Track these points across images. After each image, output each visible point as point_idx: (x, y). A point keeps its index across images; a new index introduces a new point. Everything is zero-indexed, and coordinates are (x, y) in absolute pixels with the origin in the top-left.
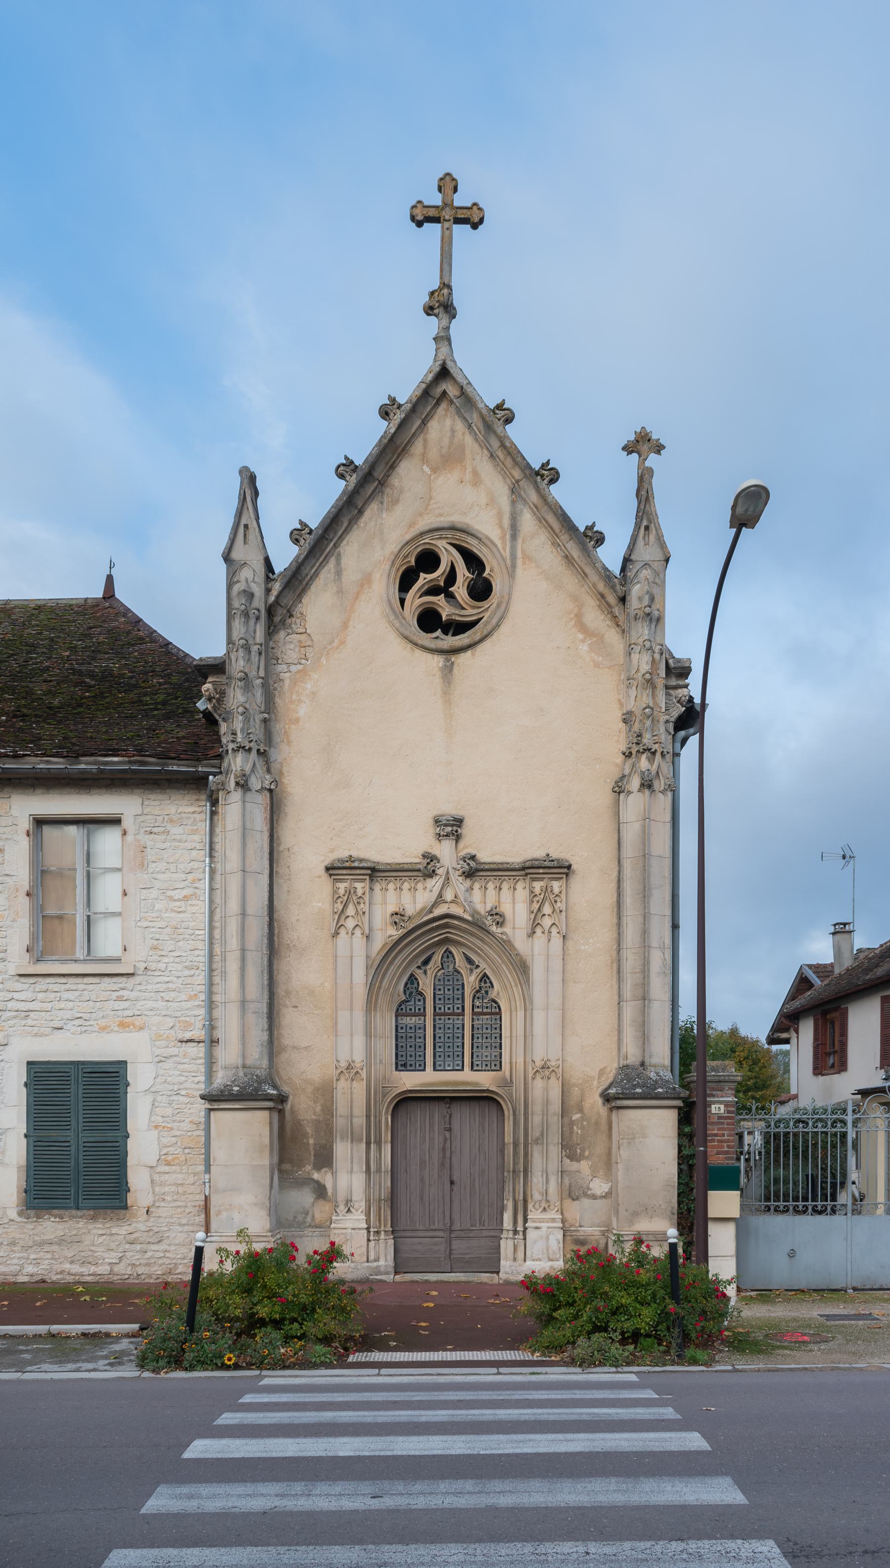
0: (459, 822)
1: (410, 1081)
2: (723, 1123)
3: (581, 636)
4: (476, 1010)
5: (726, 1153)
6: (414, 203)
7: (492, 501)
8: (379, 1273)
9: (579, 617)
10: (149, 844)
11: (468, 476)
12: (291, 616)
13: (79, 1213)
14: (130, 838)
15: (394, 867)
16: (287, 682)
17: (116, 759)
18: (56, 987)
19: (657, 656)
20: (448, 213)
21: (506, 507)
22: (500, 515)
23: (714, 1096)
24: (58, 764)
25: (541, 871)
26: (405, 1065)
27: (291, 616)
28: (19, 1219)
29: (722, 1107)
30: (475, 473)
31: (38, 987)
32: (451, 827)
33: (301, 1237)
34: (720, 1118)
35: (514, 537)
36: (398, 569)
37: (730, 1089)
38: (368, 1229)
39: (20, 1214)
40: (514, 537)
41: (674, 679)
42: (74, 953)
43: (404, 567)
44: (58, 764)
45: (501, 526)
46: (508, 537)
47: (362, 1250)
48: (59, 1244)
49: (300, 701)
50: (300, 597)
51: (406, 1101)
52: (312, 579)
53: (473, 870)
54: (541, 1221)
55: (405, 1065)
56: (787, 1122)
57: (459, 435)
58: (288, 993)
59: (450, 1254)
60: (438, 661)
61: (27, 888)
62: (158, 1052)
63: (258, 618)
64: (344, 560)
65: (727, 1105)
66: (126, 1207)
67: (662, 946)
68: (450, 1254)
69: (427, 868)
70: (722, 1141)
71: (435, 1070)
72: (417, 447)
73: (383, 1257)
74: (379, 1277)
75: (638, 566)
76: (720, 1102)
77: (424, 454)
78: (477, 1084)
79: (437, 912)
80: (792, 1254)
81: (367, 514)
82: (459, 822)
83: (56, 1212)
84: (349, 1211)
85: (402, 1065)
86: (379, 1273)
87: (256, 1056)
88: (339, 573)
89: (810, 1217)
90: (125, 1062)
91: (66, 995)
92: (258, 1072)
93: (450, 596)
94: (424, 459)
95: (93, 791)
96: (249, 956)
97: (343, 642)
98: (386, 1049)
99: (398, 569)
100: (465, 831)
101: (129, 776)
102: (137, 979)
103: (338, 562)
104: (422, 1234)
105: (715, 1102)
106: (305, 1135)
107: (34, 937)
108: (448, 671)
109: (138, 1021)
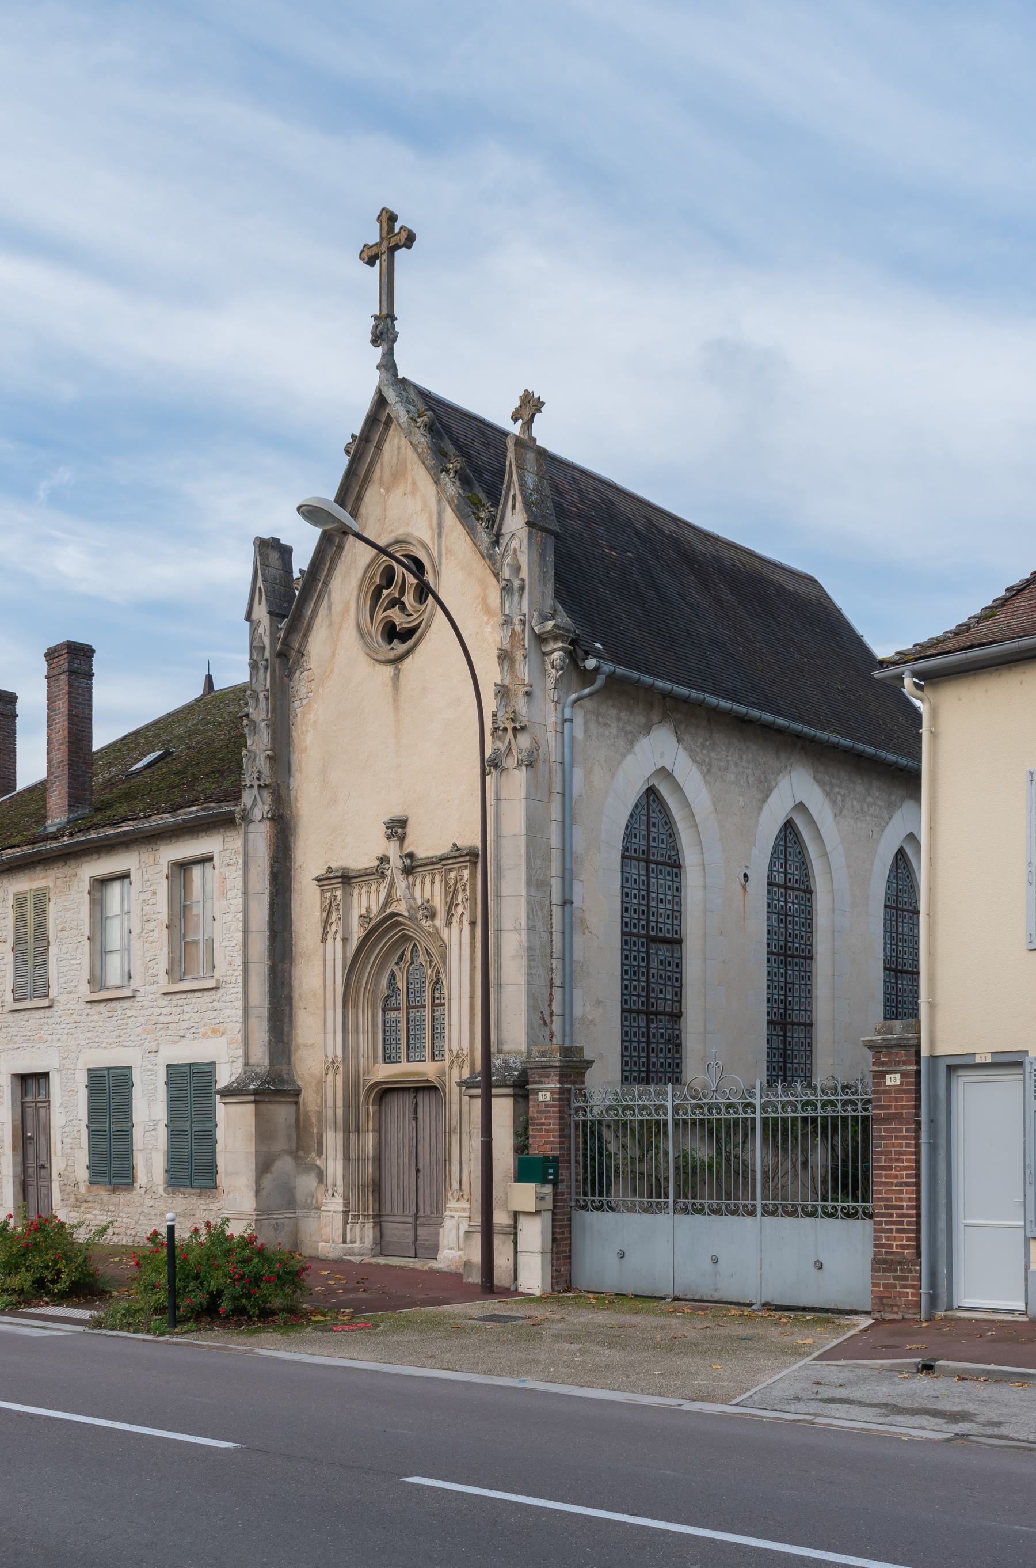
0: (403, 823)
1: (383, 1072)
2: (549, 1112)
3: (486, 618)
4: (436, 1001)
5: (552, 1143)
6: (361, 248)
7: (425, 506)
8: (352, 1254)
9: (484, 599)
10: (227, 874)
11: (409, 488)
12: (303, 655)
13: (193, 1191)
14: (217, 871)
15: (362, 872)
16: (299, 716)
17: (194, 808)
18: (180, 1003)
19: (518, 628)
20: (390, 243)
21: (434, 508)
22: (430, 518)
23: (541, 1083)
24: (167, 819)
25: (450, 861)
26: (389, 1058)
27: (303, 655)
28: (165, 1195)
29: (548, 1094)
30: (414, 483)
31: (174, 1003)
32: (397, 829)
33: (308, 1217)
34: (547, 1106)
35: (440, 535)
36: (367, 591)
37: (555, 1075)
38: (346, 1213)
39: (165, 1190)
40: (440, 535)
41: (552, 644)
42: (199, 973)
43: (373, 588)
44: (167, 819)
45: (431, 528)
46: (436, 536)
47: (331, 1230)
48: (185, 1217)
49: (307, 731)
50: (306, 636)
51: (385, 1092)
52: (313, 618)
53: (411, 866)
54: (456, 1210)
55: (389, 1058)
56: (717, 1106)
57: (403, 450)
58: (300, 996)
59: (416, 1239)
60: (388, 671)
61: (166, 922)
62: (232, 1053)
63: (266, 668)
64: (333, 595)
65: (552, 1091)
66: (216, 1187)
67: (518, 927)
68: (416, 1239)
69: (378, 872)
70: (547, 1131)
71: (409, 1061)
72: (376, 475)
73: (363, 1236)
74: (348, 1258)
75: (507, 538)
76: (547, 1089)
77: (381, 478)
78: (424, 1074)
79: (388, 911)
80: (622, 1255)
81: (347, 547)
82: (403, 823)
83: (182, 1189)
84: (333, 1195)
85: (388, 1059)
86: (352, 1254)
87: (260, 1056)
88: (330, 608)
89: (780, 1218)
90: (214, 1063)
91: (188, 1008)
92: (258, 1070)
93: (403, 607)
94: (381, 483)
95: (201, 835)
96: (252, 968)
97: (332, 671)
98: (367, 1043)
99: (367, 591)
100: (410, 829)
101: (214, 819)
102: (221, 991)
103: (329, 599)
104: (398, 1219)
105: (542, 1090)
106: (311, 1125)
107: (172, 961)
108: (396, 677)
109: (222, 1027)
